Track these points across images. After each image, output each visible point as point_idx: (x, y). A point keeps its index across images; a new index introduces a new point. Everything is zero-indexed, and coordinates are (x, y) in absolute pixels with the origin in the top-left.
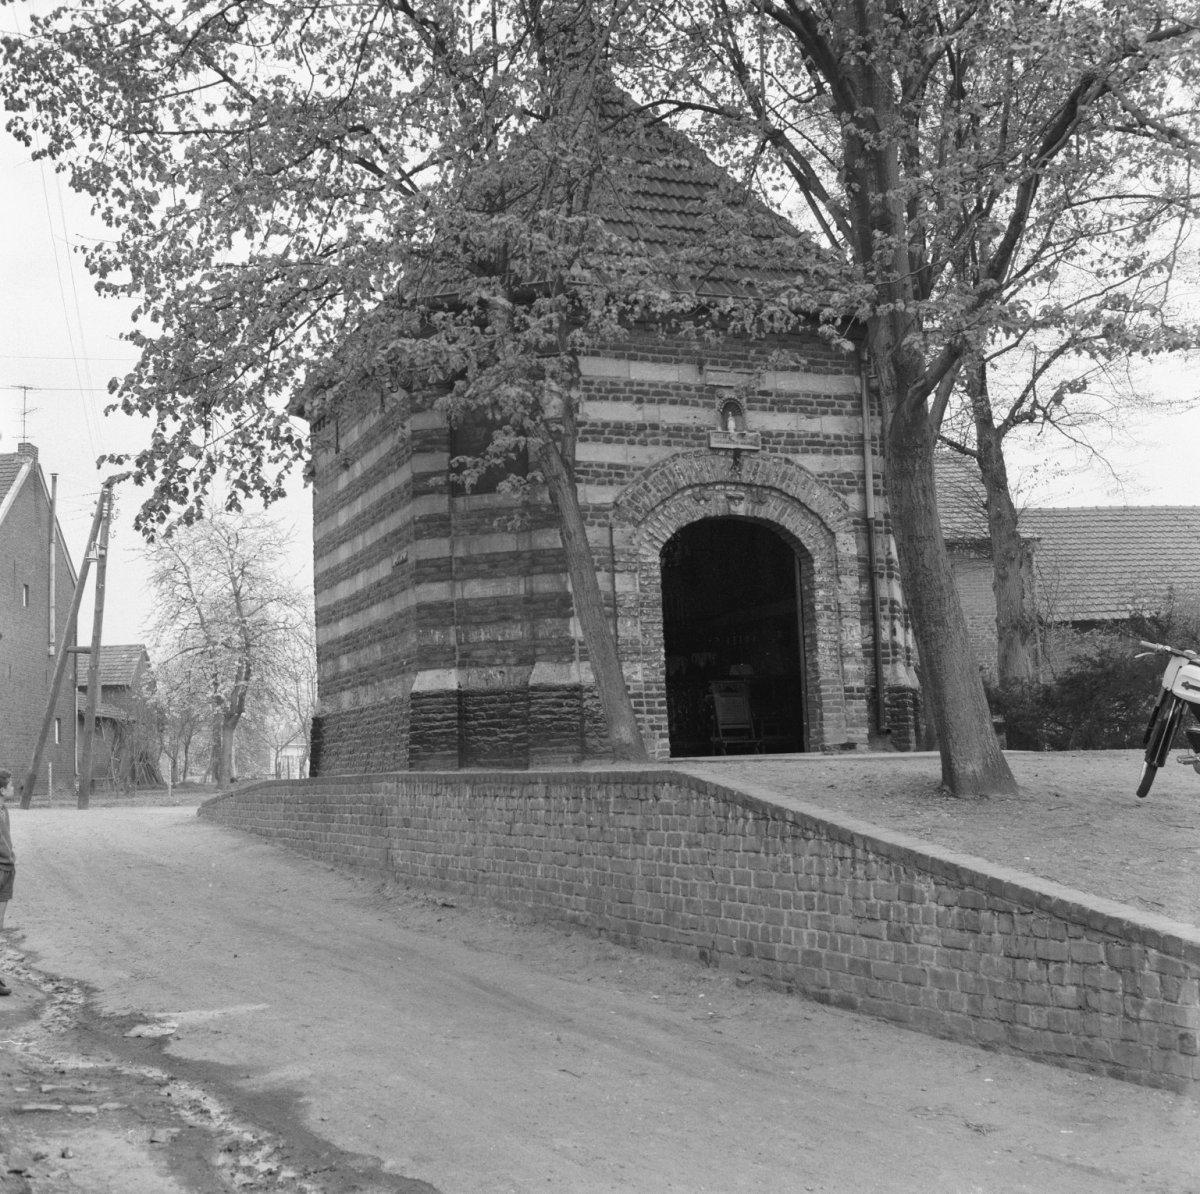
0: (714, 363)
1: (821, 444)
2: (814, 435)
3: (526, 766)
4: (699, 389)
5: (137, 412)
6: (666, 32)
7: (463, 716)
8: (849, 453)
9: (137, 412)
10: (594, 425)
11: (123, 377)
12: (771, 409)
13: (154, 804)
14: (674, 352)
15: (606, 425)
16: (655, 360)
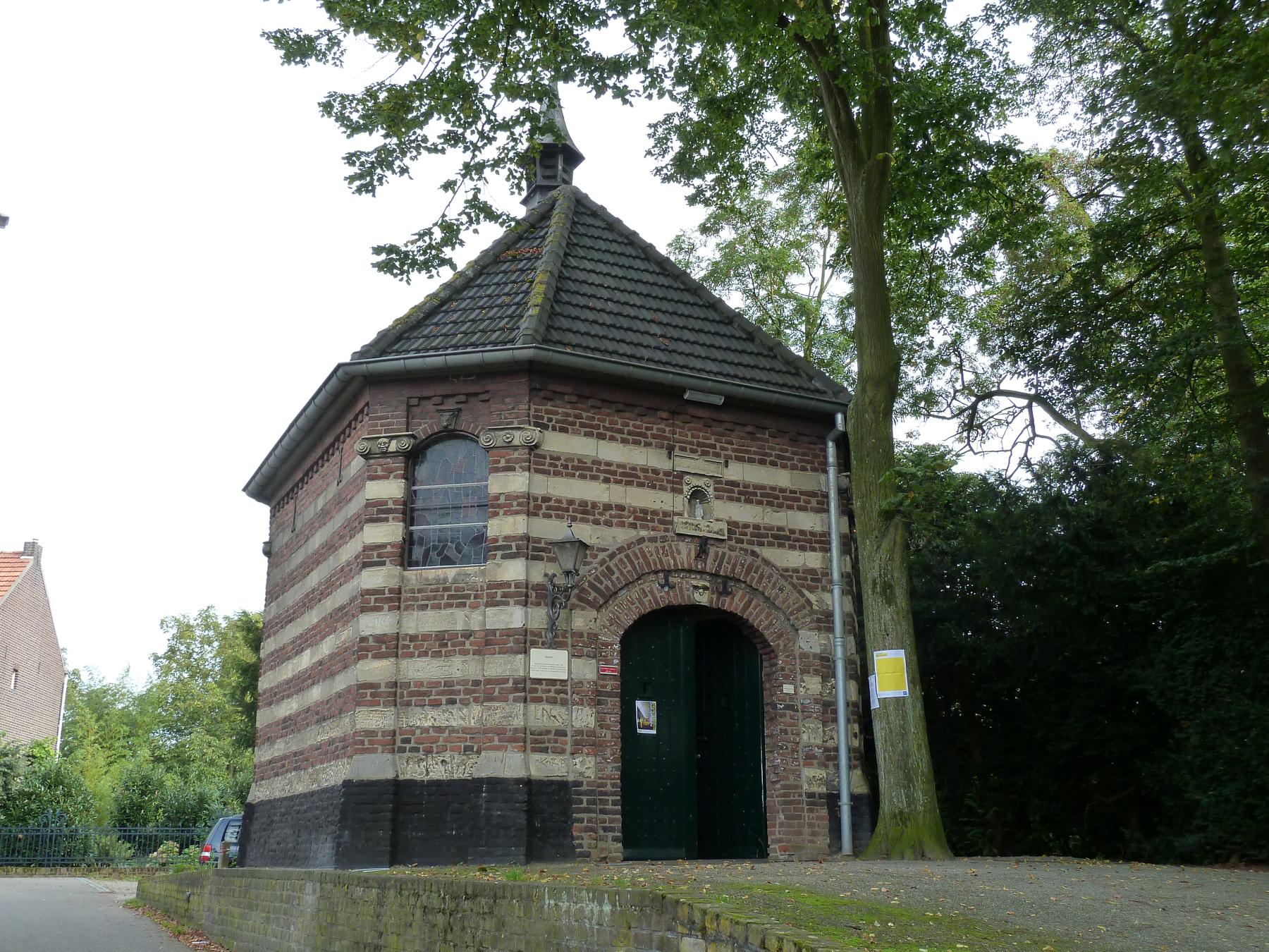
1: (788, 538)
2: (780, 529)
4: (667, 474)
8: (813, 549)
10: (558, 501)
12: (738, 500)
14: (645, 436)
15: (571, 502)
16: (624, 441)
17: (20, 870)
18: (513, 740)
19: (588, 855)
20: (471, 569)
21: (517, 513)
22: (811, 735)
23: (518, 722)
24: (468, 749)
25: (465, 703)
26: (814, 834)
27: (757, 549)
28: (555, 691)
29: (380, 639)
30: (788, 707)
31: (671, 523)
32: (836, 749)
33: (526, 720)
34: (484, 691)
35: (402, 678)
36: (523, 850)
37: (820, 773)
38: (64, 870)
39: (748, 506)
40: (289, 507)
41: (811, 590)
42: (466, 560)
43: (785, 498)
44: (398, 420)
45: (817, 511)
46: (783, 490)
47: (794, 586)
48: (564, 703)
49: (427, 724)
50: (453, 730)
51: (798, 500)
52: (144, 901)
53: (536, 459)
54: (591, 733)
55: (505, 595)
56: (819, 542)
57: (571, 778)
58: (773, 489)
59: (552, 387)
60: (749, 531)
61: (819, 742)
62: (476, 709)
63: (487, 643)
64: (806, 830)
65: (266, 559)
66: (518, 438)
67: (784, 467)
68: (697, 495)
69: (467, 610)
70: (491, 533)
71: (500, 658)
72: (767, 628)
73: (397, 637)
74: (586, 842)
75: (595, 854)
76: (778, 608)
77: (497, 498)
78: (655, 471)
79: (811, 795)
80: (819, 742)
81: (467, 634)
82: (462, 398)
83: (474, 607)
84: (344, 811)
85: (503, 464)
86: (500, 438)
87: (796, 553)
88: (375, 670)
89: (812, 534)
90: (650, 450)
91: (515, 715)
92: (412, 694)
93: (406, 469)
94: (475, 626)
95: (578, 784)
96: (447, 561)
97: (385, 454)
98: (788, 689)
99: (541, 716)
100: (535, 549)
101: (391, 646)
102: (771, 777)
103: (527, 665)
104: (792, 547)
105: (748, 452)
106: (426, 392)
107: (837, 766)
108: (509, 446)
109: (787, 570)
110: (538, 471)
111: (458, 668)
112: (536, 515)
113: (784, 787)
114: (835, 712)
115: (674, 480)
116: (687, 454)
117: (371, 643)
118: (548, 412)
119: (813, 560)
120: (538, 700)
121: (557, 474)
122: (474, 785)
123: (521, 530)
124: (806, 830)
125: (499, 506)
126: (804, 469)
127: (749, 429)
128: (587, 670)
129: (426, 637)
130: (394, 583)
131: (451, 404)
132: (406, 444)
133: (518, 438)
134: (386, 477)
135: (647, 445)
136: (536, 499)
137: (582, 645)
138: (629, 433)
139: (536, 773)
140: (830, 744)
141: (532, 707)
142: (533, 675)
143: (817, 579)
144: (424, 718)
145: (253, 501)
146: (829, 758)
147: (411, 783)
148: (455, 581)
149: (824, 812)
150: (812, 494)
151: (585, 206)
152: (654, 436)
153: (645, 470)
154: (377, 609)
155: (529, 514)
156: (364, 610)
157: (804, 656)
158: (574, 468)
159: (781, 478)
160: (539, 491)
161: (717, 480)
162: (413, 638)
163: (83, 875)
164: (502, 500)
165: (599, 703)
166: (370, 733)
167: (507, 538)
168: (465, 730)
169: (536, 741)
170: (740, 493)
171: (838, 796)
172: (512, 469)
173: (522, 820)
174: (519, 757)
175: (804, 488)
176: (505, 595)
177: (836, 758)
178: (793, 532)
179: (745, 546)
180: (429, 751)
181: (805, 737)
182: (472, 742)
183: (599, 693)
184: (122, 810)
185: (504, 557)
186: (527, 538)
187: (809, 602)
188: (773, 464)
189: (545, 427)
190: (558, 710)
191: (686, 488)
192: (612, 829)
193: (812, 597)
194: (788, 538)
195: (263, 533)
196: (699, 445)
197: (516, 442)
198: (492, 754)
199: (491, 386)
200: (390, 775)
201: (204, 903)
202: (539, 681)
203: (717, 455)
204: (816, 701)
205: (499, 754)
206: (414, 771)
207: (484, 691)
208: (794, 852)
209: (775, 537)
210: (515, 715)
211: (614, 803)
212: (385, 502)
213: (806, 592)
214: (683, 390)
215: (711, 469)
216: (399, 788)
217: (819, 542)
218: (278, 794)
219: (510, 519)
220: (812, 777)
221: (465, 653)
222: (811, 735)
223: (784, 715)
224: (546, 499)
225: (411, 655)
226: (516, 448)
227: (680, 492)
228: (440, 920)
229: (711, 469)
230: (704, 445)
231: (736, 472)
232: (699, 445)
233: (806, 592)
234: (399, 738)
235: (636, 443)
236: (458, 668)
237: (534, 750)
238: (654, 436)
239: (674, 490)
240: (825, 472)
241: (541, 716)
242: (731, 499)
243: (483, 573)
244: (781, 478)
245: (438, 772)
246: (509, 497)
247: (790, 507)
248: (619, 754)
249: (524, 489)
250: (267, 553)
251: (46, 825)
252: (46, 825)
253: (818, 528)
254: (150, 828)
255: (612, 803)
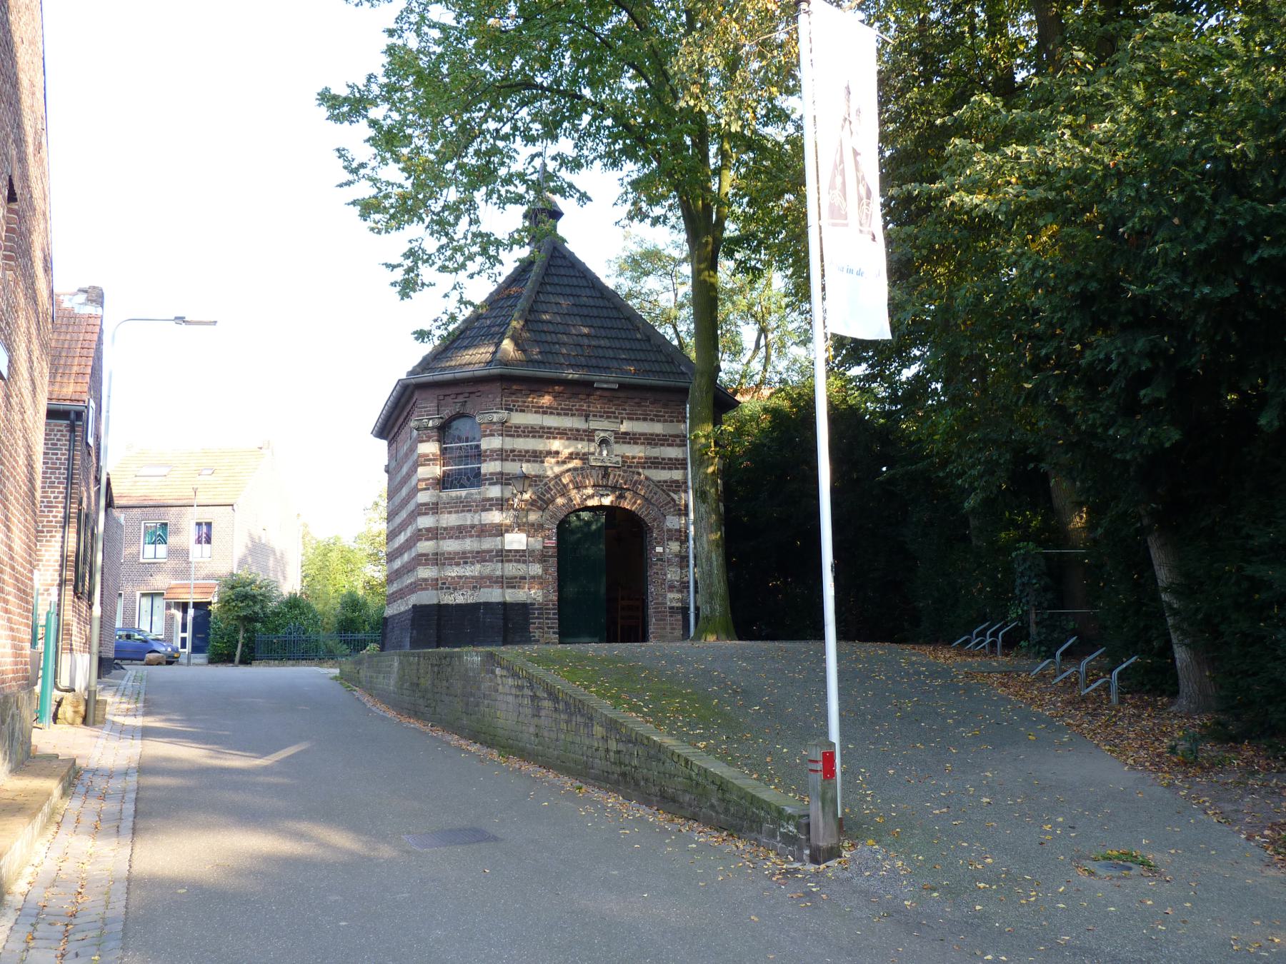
0: (594, 416)
1: (661, 463)
2: (655, 458)
3: (144, 769)
4: (585, 431)
5: (467, 263)
6: (736, 97)
7: (506, 619)
8: (677, 469)
9: (467, 263)
10: (520, 451)
11: (614, 174)
12: (629, 443)
13: (181, 760)
14: (571, 410)
15: (527, 452)
16: (558, 414)
17: (276, 662)
18: (496, 582)
19: (538, 641)
20: (474, 491)
21: (496, 460)
22: (673, 575)
23: (499, 573)
24: (475, 587)
25: (473, 564)
26: (673, 629)
27: (641, 470)
28: (520, 556)
29: (428, 530)
30: (658, 560)
31: (588, 459)
32: (688, 582)
33: (503, 571)
34: (481, 557)
35: (440, 551)
36: (501, 638)
37: (678, 596)
38: (304, 662)
39: (635, 446)
40: (394, 445)
41: (675, 492)
42: (472, 486)
43: (659, 440)
44: (431, 406)
45: (679, 446)
46: (657, 435)
47: (663, 491)
48: (524, 562)
49: (454, 574)
50: (467, 577)
51: (668, 440)
52: (343, 678)
53: (507, 430)
54: (540, 577)
55: (491, 505)
56: (679, 464)
57: (529, 601)
58: (652, 435)
59: (514, 387)
60: (635, 461)
61: (678, 578)
62: (478, 566)
63: (482, 531)
64: (668, 627)
65: (386, 475)
66: (495, 418)
67: (659, 421)
68: (604, 442)
69: (472, 514)
70: (483, 471)
71: (489, 539)
72: (647, 515)
73: (437, 528)
74: (537, 635)
75: (542, 640)
76: (653, 504)
77: (486, 451)
78: (578, 430)
79: (672, 608)
80: (678, 578)
81: (473, 527)
82: (467, 395)
83: (476, 512)
84: (413, 620)
85: (488, 432)
86: (487, 418)
87: (666, 471)
88: (425, 546)
89: (676, 459)
90: (575, 419)
91: (496, 569)
92: (445, 559)
93: (439, 436)
94: (476, 522)
95: (532, 604)
96: (463, 486)
97: (427, 428)
98: (659, 549)
99: (511, 569)
100: (506, 479)
101: (434, 534)
102: (650, 599)
103: (503, 543)
104: (664, 468)
105: (636, 414)
106: (448, 392)
107: (688, 592)
108: (491, 423)
109: (659, 482)
110: (507, 436)
111: (469, 544)
112: (507, 460)
113: (656, 604)
114: (688, 561)
115: (589, 435)
116: (598, 419)
117: (424, 532)
118: (513, 401)
119: (677, 475)
120: (510, 561)
121: (519, 436)
122: (476, 606)
123: (498, 469)
124: (668, 627)
125: (488, 456)
126: (672, 421)
127: (637, 400)
128: (537, 543)
129: (452, 528)
130: (434, 500)
131: (461, 399)
132: (437, 422)
133: (495, 418)
134: (428, 441)
135: (572, 415)
136: (506, 451)
137: (531, 529)
138: (562, 409)
139: (508, 599)
140: (685, 579)
141: (506, 565)
142: (507, 547)
143: (679, 486)
144: (453, 572)
145: (378, 440)
146: (684, 587)
147: (447, 605)
148: (466, 497)
149: (680, 617)
150: (677, 436)
151: (558, 251)
152: (577, 410)
153: (571, 430)
154: (426, 514)
155: (502, 460)
156: (421, 514)
157: (669, 530)
158: (529, 432)
159: (657, 428)
160: (508, 446)
161: (616, 433)
162: (445, 529)
163: (316, 665)
164: (488, 453)
165: (545, 561)
166: (425, 580)
167: (491, 474)
168: (473, 577)
169: (512, 582)
170: (630, 439)
171: (688, 609)
172: (493, 435)
173: (501, 623)
174: (500, 591)
175: (671, 433)
176: (491, 505)
177: (688, 587)
178: (663, 459)
179: (633, 469)
180: (455, 589)
181: (669, 576)
182: (478, 583)
183: (545, 556)
184: (340, 622)
185: (490, 484)
186: (502, 473)
187: (673, 500)
188: (652, 420)
189: (511, 410)
190: (521, 566)
191: (596, 438)
192: (553, 628)
193: (676, 497)
194: (661, 463)
195: (384, 460)
196: (605, 412)
197: (495, 420)
198: (486, 590)
199: (481, 388)
200: (435, 602)
201: (364, 673)
202: (510, 551)
203: (617, 418)
204: (676, 556)
205: (490, 590)
206: (449, 599)
207: (481, 557)
208: (662, 638)
209: (652, 463)
210: (496, 569)
211: (554, 614)
212: (428, 455)
213: (672, 494)
214: (594, 383)
215: (613, 427)
216: (440, 608)
217: (679, 464)
218: (396, 612)
219: (493, 463)
220: (673, 598)
221: (471, 536)
222: (673, 575)
223: (656, 564)
224: (512, 451)
225: (445, 538)
226: (495, 423)
227: (594, 441)
228: (436, 669)
229: (613, 427)
230: (608, 412)
231: (625, 427)
232: (605, 412)
233: (672, 494)
234: (440, 582)
235: (566, 415)
236: (469, 544)
237: (508, 587)
238: (577, 410)
239: (589, 440)
240: (685, 422)
241: (511, 569)
242: (624, 443)
243: (480, 493)
244: (657, 428)
245: (460, 600)
246: (492, 451)
247: (662, 445)
248: (556, 588)
249: (500, 446)
250: (387, 471)
251: (290, 634)
252: (290, 634)
253: (680, 456)
254: (361, 636)
255: (553, 614)
